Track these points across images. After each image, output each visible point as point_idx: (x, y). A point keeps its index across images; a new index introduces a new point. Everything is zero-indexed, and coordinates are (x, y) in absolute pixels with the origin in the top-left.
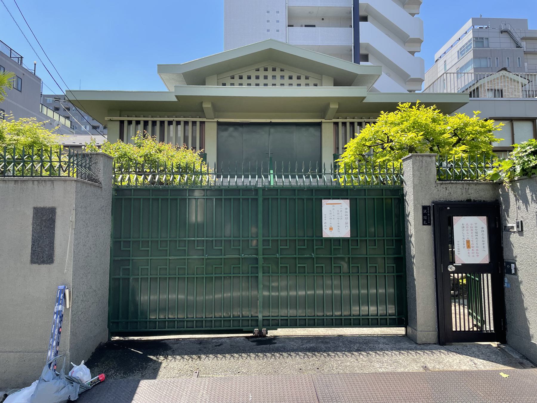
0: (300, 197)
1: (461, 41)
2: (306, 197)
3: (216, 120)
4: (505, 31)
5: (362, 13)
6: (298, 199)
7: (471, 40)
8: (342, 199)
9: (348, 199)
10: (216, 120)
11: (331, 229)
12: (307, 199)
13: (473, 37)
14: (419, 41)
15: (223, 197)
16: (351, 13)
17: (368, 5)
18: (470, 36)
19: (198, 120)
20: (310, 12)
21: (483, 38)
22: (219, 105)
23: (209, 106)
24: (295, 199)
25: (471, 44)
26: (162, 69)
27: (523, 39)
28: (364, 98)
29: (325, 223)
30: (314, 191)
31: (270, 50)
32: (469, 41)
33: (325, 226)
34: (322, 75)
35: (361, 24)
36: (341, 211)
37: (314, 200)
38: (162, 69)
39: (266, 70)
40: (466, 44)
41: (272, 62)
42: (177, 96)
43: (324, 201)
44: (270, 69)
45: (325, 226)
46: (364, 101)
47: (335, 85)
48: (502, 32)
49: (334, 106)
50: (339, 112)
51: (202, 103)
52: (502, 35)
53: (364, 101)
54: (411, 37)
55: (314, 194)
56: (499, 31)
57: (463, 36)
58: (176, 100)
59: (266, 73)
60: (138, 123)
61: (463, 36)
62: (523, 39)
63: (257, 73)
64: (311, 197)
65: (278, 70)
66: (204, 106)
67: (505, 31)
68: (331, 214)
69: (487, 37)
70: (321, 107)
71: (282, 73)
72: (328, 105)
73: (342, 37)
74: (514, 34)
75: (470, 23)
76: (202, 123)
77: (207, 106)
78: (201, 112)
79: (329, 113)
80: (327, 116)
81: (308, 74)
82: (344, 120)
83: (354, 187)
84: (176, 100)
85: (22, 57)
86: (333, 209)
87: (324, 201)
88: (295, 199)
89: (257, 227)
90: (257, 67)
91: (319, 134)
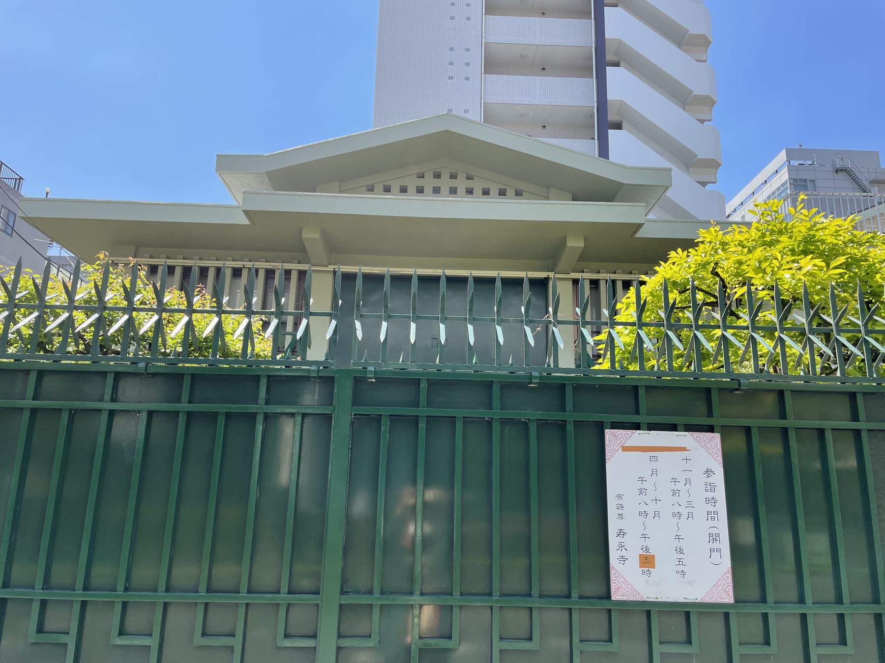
0: (509, 414)
1: (768, 185)
2: (539, 414)
3: (331, 268)
4: (842, 170)
5: (612, 117)
6: (504, 422)
7: (785, 183)
8: (689, 428)
9: (711, 429)
10: (331, 268)
11: (647, 561)
12: (543, 424)
13: (790, 179)
14: (714, 164)
15: (184, 406)
16: (593, 116)
17: (622, 103)
18: (784, 176)
19: (295, 267)
20: (521, 115)
21: (805, 181)
22: (341, 237)
23: (317, 236)
24: (490, 423)
25: (787, 188)
26: (225, 163)
27: (873, 182)
28: (640, 226)
29: (621, 533)
30: (569, 391)
31: (446, 132)
32: (783, 185)
33: (621, 546)
34: (549, 189)
35: (611, 132)
36: (688, 482)
37: (570, 428)
38: (225, 163)
39: (437, 176)
40: (778, 189)
41: (446, 158)
42: (246, 212)
43: (610, 435)
44: (445, 176)
45: (621, 546)
46: (640, 234)
47: (574, 199)
48: (837, 171)
49: (575, 243)
50: (585, 258)
51: (301, 230)
52: (836, 176)
53: (640, 234)
54: (700, 156)
55: (569, 404)
56: (831, 169)
57: (771, 177)
58: (245, 221)
59: (437, 183)
60: (171, 270)
61: (771, 177)
62: (873, 182)
63: (420, 182)
64: (558, 416)
65: (461, 177)
66: (305, 235)
67: (842, 170)
68: (641, 492)
69: (813, 178)
70: (547, 246)
71: (470, 184)
72: (564, 240)
73: (576, 93)
74: (858, 175)
75: (782, 156)
76: (302, 274)
77: (311, 235)
78: (301, 252)
79: (565, 260)
80: (560, 267)
81: (520, 185)
82: (595, 276)
83: (737, 379)
84: (245, 221)
85: (21, 178)
86: (654, 472)
87: (610, 435)
88: (490, 423)
89: (349, 523)
90: (419, 170)
91: (544, 303)
